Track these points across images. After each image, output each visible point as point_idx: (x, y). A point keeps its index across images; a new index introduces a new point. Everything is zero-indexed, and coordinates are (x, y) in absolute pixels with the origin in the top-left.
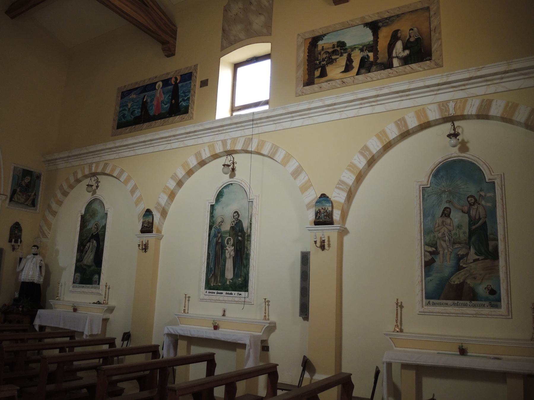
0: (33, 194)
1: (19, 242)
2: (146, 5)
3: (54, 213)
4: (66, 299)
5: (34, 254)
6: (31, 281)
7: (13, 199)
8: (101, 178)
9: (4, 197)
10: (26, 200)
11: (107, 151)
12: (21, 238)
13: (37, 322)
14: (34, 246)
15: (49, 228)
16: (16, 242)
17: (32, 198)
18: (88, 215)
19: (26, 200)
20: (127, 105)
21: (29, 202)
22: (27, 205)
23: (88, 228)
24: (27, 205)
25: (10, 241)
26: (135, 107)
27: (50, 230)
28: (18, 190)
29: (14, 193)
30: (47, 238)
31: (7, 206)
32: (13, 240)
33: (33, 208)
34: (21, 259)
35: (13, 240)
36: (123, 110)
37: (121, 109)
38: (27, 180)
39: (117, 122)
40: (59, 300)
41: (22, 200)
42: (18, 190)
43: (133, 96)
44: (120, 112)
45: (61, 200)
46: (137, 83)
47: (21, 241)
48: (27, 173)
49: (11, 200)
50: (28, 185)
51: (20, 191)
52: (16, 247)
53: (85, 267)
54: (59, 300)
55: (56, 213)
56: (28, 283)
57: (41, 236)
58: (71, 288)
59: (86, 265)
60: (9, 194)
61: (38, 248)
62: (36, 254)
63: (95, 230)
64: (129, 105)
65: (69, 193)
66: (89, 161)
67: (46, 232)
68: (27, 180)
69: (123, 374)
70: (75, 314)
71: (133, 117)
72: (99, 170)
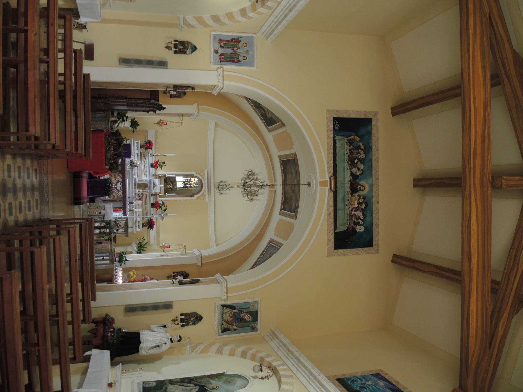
0: (235, 328)
1: (182, 324)
2: (490, 344)
3: (219, 352)
4: (123, 381)
5: (171, 339)
6: (141, 340)
7: (225, 308)
8: (274, 378)
9: (225, 298)
10: (227, 322)
11: (306, 372)
12: (186, 325)
13: (94, 352)
14: (180, 337)
15: (202, 352)
16: (182, 321)
17: (230, 327)
18: (227, 377)
19: (227, 322)
20: (368, 381)
21: (226, 326)
22: (222, 324)
23: (212, 381)
24: (222, 324)
25: (181, 315)
26: (370, 387)
27: (200, 353)
28: (236, 311)
29: (232, 307)
30: (192, 352)
31: (217, 303)
32: (183, 317)
33: (220, 331)
34: (165, 326)
35: (183, 317)
36: (360, 379)
37: (361, 377)
38: (248, 318)
39: (343, 377)
40: (123, 373)
41: (226, 318)
42: (236, 311)
43: (382, 383)
44: (356, 377)
45: (236, 353)
46: (398, 383)
47: (182, 326)
48: (254, 315)
49: (223, 306)
50: (242, 320)
51: (234, 313)
52: (176, 323)
53: (164, 388)
54: (123, 373)
55: (221, 354)
56: (140, 338)
57: (192, 345)
58: (137, 381)
59: (166, 388)
60: (228, 303)
61: (179, 341)
62: (172, 341)
63: (211, 388)
64: (369, 383)
65: (246, 358)
66: (288, 362)
67: (197, 348)
68: (248, 318)
69: (35, 104)
70: (106, 385)
71: (358, 389)
72: (281, 373)
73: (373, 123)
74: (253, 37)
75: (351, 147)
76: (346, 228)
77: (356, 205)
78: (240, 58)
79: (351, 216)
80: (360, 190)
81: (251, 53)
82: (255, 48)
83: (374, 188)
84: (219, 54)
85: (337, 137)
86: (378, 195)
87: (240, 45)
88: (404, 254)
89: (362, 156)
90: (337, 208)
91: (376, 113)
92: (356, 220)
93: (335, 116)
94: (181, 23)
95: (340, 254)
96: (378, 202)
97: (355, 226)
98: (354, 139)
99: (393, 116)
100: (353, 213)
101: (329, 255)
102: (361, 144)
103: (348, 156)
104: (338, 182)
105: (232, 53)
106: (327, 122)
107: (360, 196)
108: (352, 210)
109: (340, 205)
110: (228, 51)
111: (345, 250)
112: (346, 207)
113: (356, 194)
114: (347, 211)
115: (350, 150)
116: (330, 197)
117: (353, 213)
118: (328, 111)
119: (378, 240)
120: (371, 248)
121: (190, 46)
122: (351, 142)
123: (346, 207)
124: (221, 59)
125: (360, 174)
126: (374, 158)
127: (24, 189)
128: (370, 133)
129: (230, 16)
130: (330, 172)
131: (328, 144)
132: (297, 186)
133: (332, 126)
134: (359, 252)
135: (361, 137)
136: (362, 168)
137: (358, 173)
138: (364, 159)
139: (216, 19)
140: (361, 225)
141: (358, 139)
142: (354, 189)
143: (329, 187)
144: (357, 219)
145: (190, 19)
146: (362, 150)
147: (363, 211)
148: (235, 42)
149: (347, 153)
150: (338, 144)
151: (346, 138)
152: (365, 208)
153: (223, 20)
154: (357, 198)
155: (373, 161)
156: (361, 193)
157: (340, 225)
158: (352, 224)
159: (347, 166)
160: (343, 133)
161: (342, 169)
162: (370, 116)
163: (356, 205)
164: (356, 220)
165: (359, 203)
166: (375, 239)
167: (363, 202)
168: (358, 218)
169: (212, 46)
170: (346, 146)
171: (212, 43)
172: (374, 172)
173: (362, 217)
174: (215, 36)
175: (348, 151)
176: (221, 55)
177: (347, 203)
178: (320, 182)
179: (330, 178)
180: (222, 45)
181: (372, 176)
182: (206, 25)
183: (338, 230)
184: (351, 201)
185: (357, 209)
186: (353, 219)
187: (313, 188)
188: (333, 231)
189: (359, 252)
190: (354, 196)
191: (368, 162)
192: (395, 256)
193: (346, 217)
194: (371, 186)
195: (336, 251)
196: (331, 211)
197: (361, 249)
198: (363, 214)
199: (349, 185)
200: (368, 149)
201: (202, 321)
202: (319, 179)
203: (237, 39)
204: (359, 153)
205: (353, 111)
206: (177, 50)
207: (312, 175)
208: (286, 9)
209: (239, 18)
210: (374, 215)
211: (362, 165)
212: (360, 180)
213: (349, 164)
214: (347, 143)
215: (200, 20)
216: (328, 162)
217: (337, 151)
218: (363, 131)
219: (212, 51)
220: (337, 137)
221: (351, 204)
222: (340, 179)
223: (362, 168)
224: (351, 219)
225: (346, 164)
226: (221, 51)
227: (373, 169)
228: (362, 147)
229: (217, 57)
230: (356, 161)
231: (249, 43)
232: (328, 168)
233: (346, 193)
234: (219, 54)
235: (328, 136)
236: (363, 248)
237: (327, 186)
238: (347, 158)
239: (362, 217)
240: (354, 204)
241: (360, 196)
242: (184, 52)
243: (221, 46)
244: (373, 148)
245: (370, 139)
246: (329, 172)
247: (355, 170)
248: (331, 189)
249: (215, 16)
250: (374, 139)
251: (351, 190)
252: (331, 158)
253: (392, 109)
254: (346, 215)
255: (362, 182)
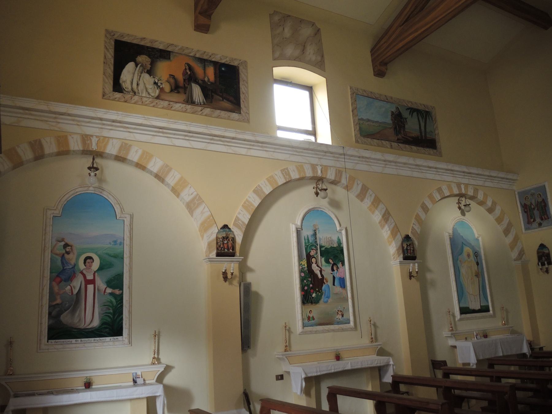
74: (518, 193)
78: (540, 200)
81: (533, 191)
82: (528, 188)
84: (541, 222)
87: (528, 203)
94: (520, 262)
105: (538, 209)
110: (536, 213)
121: (541, 251)
124: (546, 219)
129: (499, 220)
139: (507, 232)
145: (514, 254)
148: (527, 209)
153: (505, 226)
169: (536, 230)
171: (533, 230)
174: (526, 229)
176: (542, 219)
180: (532, 220)
182: (516, 239)
201: (545, 243)
203: (523, 207)
206: (546, 263)
208: (471, 177)
209: (498, 211)
215: (513, 246)
219: (540, 229)
226: (538, 220)
229: (544, 223)
231: (523, 195)
234: (541, 222)
242: (548, 255)
243: (534, 221)
249: (505, 233)
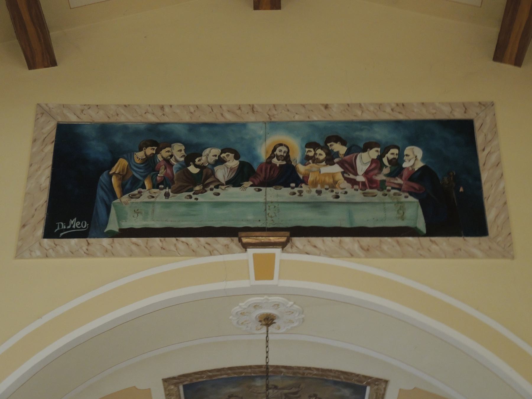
73: (73, 119)
75: (147, 183)
76: (411, 199)
77: (336, 169)
79: (370, 183)
80: (287, 158)
83: (281, 116)
85: (113, 226)
86: (303, 106)
88: (494, 31)
89: (178, 152)
90: (346, 225)
91: (43, 111)
92: (386, 171)
93: (40, 231)
95: (502, 217)
96: (326, 107)
97: (405, 173)
98: (122, 177)
99: (53, 63)
100: (360, 178)
101: (507, 252)
102: (140, 155)
103: (177, 191)
104: (260, 225)
106: (58, 256)
107: (306, 159)
108: (353, 182)
109: (335, 218)
111: (487, 204)
112: (343, 198)
113: (301, 169)
114: (357, 195)
115: (155, 186)
116: (309, 248)
117: (360, 178)
118: (19, 254)
119: (450, 104)
120: (477, 125)
122: (131, 185)
123: (343, 198)
125: (237, 157)
126: (186, 118)
127: (267, 223)
128: (105, 130)
130: (227, 246)
131: (131, 254)
132: (273, 381)
133: (74, 241)
134: (493, 159)
135: (116, 154)
136: (216, 151)
137: (233, 163)
138: (188, 146)
140: (401, 155)
141: (122, 163)
142: (283, 175)
143: (277, 251)
144: (383, 165)
146: (158, 152)
147: (355, 149)
149: (167, 195)
150: (137, 223)
151: (115, 197)
152: (344, 143)
154: (312, 165)
155: (194, 120)
156: (296, 156)
157: (402, 218)
158: (399, 181)
159: (209, 196)
160: (100, 208)
161: (219, 212)
162: (50, 129)
163: (336, 169)
164: (386, 171)
165: (330, 159)
166: (445, 114)
167: (325, 148)
168: (378, 163)
170: (145, 197)
172: (230, 118)
173: (374, 153)
175: (160, 195)
177: (328, 196)
178: (257, 278)
179: (246, 246)
181: (244, 125)
183: (422, 225)
184: (323, 184)
185: (349, 167)
186: (380, 177)
187: (277, 305)
188: (426, 241)
189: (493, 159)
190: (306, 177)
191: (195, 137)
192: (499, 56)
193: (375, 199)
194: (274, 125)
195: (492, 229)
196: (356, 246)
197: (482, 156)
198: (364, 150)
199: (271, 191)
200: (157, 135)
202: (249, 282)
204: (167, 161)
205: (29, 177)
207: (237, 309)
210: (367, 117)
211: (207, 151)
212: (256, 158)
213: (203, 191)
214: (132, 197)
216: (195, 253)
217: (157, 225)
218: (97, 149)
220: (113, 226)
221: (333, 185)
222: (250, 217)
223: (216, 151)
224: (382, 186)
225: (201, 198)
227: (220, 120)
228: (150, 151)
230: (193, 170)
232: (211, 254)
233: (296, 198)
235: (106, 252)
236: (479, 148)
237: (274, 255)
238: (182, 197)
239: (374, 153)
240: (333, 175)
241: (306, 159)
244: (152, 119)
245: (124, 128)
246: (228, 250)
247: (222, 174)
248: (283, 245)
250: (125, 118)
251: (287, 185)
252: (181, 246)
253: (31, 66)
254: (367, 199)
255: (262, 153)
